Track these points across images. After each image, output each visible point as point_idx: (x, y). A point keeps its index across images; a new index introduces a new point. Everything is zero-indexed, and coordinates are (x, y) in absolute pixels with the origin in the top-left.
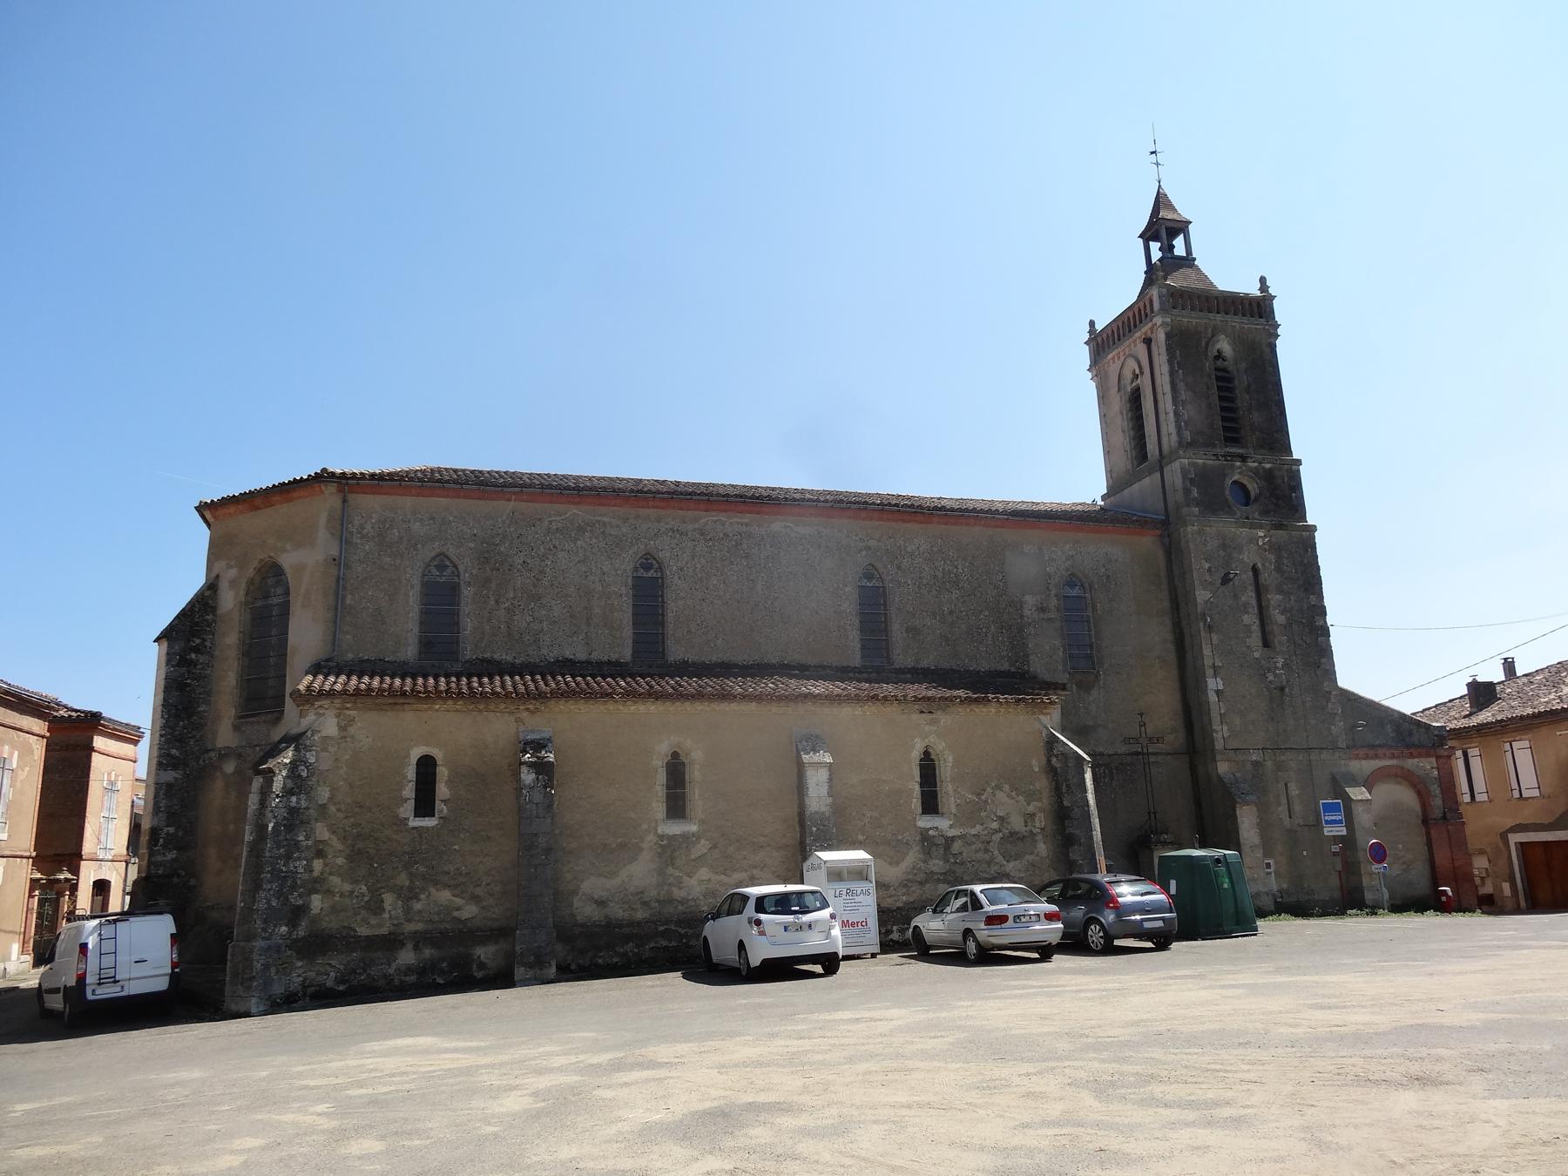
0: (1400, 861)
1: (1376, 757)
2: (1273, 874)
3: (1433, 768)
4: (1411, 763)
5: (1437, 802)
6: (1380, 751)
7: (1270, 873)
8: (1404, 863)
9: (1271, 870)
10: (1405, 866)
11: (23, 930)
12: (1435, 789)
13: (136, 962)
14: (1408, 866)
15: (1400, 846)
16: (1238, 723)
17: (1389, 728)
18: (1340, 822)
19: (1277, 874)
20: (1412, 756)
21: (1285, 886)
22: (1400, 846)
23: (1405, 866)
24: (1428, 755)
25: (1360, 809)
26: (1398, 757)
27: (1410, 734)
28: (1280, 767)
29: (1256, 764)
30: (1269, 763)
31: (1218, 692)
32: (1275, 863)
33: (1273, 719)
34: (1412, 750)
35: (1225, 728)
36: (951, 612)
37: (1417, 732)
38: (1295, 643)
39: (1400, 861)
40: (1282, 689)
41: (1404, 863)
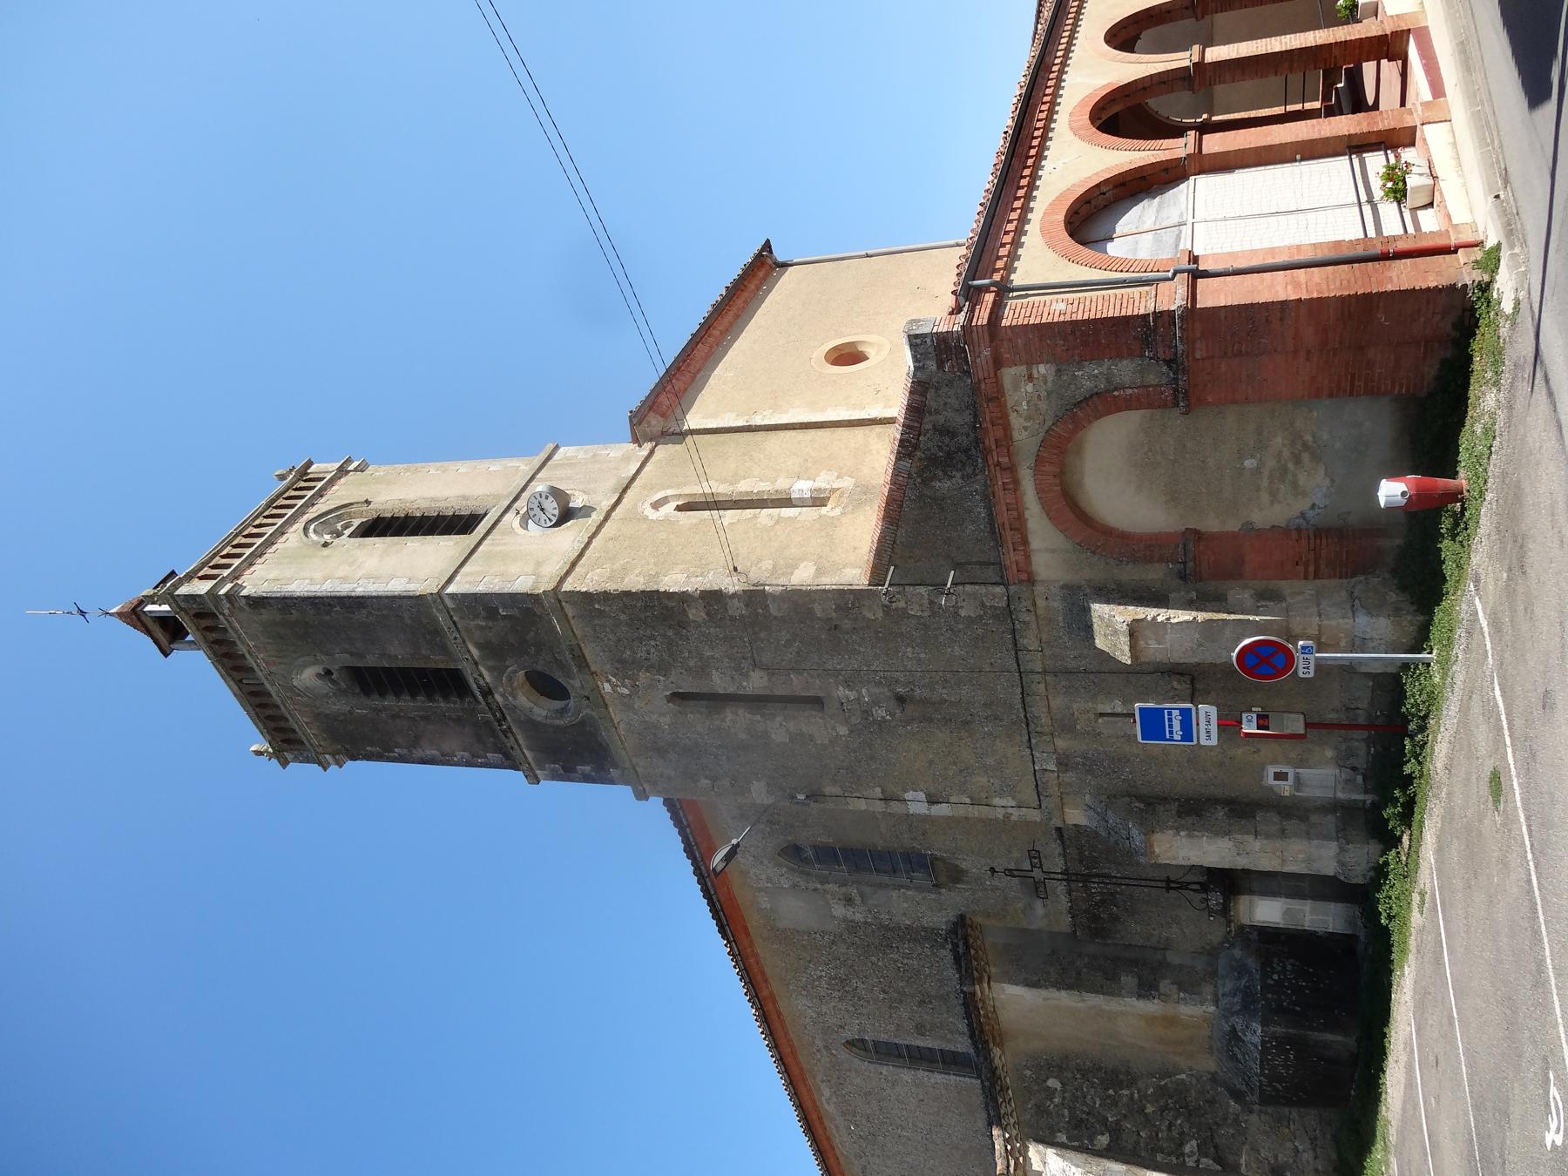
0: (1291, 466)
1: (1019, 525)
2: (1297, 770)
3: (1030, 378)
4: (1025, 432)
5: (1125, 371)
6: (1004, 517)
7: (1297, 778)
8: (1298, 461)
9: (1291, 772)
10: (1306, 457)
11: (1333, 785)
12: (1090, 376)
13: (1403, 104)
14: (1305, 446)
15: (1249, 463)
16: (984, 780)
17: (943, 486)
18: (1186, 714)
19: (1302, 763)
20: (1006, 441)
21: (1329, 753)
22: (1249, 463)
23: (1306, 457)
24: (997, 397)
25: (1153, 645)
26: (1012, 469)
27: (945, 431)
28: (1066, 726)
29: (1064, 763)
30: (1060, 743)
31: (932, 801)
32: (1275, 762)
33: (966, 723)
34: (990, 442)
35: (997, 801)
36: (884, 992)
37: (937, 412)
38: (794, 454)
39: (1291, 466)
40: (901, 700)
41: (1298, 461)
